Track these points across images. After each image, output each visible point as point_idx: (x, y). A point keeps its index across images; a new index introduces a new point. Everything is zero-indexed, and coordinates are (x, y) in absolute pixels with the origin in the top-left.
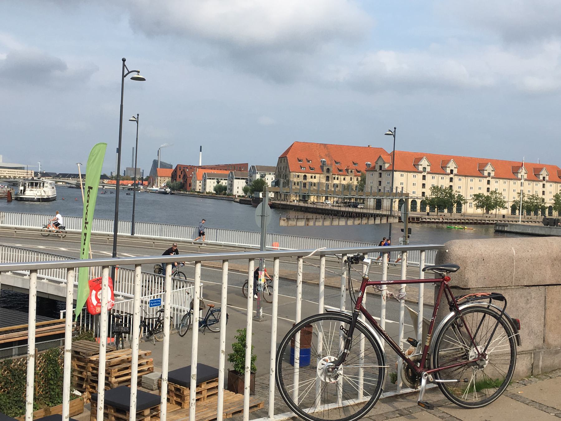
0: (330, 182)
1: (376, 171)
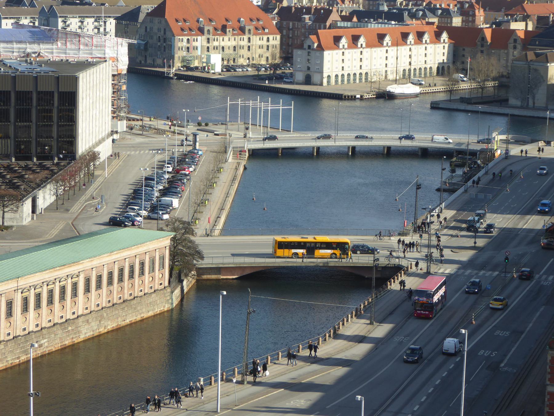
0: (211, 44)
1: (305, 49)
